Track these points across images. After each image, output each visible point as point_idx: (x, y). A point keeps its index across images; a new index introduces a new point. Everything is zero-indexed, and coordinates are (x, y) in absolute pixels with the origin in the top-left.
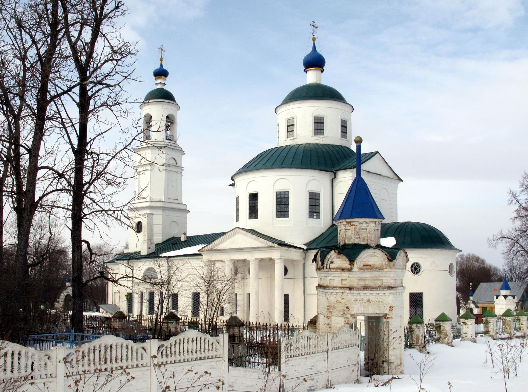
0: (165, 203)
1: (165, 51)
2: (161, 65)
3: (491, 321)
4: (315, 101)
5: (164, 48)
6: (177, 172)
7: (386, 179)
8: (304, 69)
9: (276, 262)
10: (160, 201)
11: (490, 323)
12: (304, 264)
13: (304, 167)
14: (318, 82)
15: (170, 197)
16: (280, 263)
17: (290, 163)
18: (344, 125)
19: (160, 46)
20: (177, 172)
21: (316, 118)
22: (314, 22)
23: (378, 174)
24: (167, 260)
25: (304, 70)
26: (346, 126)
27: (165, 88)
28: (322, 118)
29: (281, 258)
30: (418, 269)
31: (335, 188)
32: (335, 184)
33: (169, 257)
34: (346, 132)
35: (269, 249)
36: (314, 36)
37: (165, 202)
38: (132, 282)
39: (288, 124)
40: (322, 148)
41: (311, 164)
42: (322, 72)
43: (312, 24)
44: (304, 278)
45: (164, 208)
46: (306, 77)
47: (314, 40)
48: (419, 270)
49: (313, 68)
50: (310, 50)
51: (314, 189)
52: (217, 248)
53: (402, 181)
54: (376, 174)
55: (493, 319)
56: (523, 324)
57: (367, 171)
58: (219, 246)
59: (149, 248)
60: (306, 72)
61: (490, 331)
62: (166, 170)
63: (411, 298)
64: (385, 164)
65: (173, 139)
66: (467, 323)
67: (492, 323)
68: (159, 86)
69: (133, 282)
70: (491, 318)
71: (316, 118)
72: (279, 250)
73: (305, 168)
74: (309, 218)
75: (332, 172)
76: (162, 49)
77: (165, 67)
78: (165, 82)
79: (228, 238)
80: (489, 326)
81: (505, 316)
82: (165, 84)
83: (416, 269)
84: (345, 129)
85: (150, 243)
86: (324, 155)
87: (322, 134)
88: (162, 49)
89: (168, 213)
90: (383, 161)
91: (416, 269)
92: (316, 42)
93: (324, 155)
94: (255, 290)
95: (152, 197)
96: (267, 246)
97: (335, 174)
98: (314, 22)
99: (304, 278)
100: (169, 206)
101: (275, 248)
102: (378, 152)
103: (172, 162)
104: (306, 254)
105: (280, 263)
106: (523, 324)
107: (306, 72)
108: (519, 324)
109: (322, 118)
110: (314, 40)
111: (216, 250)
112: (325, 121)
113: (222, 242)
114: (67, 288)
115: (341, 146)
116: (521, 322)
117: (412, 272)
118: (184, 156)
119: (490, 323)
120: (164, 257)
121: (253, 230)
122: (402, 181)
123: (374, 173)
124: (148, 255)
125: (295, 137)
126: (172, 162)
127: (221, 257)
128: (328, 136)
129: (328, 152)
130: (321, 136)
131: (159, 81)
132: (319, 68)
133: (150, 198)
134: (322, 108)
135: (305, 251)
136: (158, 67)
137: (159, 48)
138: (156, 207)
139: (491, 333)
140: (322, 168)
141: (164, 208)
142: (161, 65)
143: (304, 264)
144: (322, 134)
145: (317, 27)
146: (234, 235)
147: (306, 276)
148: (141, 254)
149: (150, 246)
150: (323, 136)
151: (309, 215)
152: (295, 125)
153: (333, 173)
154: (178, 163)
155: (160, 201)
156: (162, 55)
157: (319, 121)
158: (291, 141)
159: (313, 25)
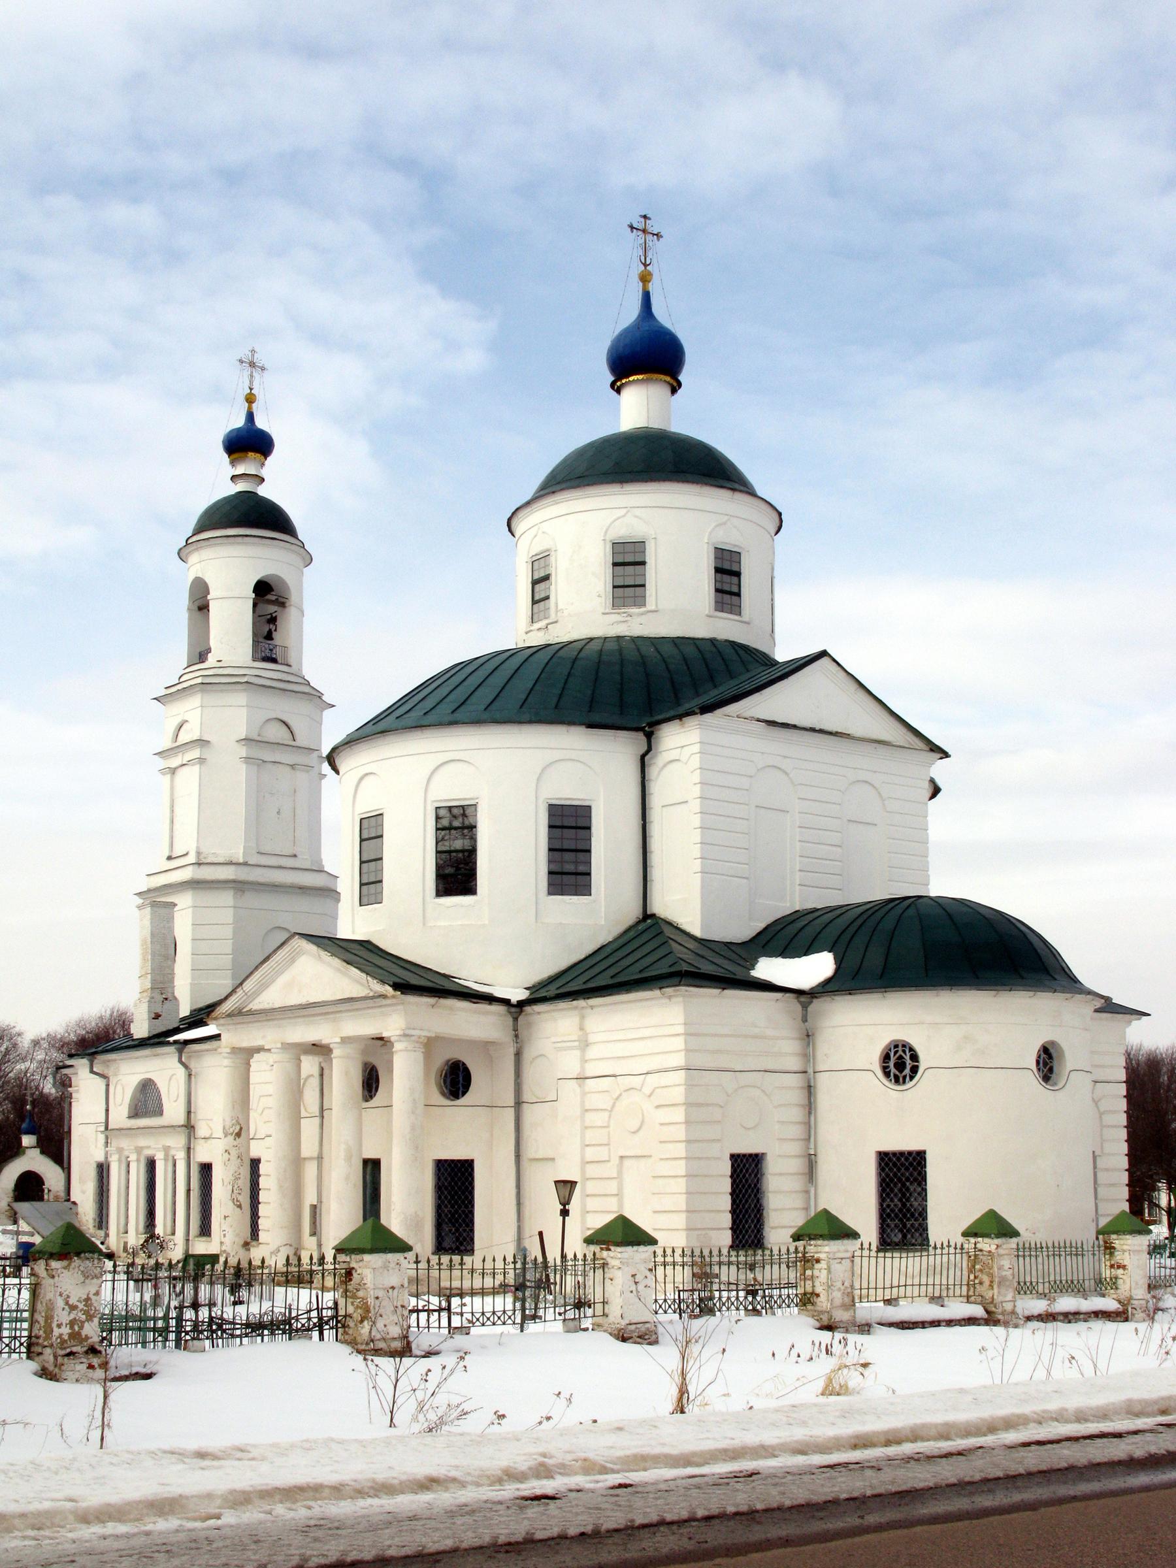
0: (246, 869)
1: (263, 369)
2: (250, 417)
3: (822, 1256)
4: (615, 488)
5: (259, 359)
6: (292, 766)
7: (870, 748)
8: (612, 379)
9: (398, 1046)
10: (231, 863)
11: (818, 1261)
12: (518, 1055)
13: (527, 717)
14: (656, 424)
15: (267, 848)
16: (406, 1050)
17: (483, 707)
18: (727, 566)
19: (244, 353)
20: (292, 766)
21: (618, 546)
22: (645, 217)
23: (830, 733)
24: (180, 1052)
25: (613, 385)
26: (735, 568)
27: (263, 491)
28: (735, 556)
29: (405, 1035)
30: (891, 1064)
31: (655, 789)
32: (653, 772)
33: (187, 1042)
34: (735, 589)
35: (370, 1003)
36: (645, 265)
37: (245, 864)
38: (103, 1129)
39: (536, 577)
40: (644, 650)
41: (556, 707)
42: (674, 391)
43: (638, 223)
44: (518, 1104)
45: (239, 886)
46: (619, 404)
47: (645, 278)
48: (914, 1070)
49: (640, 377)
50: (630, 313)
51: (569, 792)
52: (255, 1005)
53: (945, 755)
54: (821, 731)
55: (827, 1249)
56: (1124, 1267)
57: (771, 723)
58: (257, 1001)
59: (157, 1016)
60: (618, 391)
61: (818, 1295)
62: (248, 759)
63: (920, 1173)
64: (861, 694)
65: (285, 656)
66: (609, 1260)
67: (823, 1265)
68: (241, 487)
69: (107, 1128)
70: (819, 1242)
71: (618, 546)
72: (400, 1007)
73: (530, 722)
74: (551, 893)
75: (637, 729)
76: (252, 364)
77: (261, 423)
78: (264, 473)
79: (280, 973)
80: (816, 1273)
81: (976, 1235)
82: (263, 480)
83: (900, 1065)
84: (735, 579)
85: (160, 998)
86: (622, 674)
87: (640, 601)
88: (252, 364)
89: (252, 900)
90: (853, 686)
91: (900, 1065)
92: (654, 288)
93: (622, 674)
94: (343, 1147)
95: (203, 849)
96: (371, 994)
97: (649, 736)
98: (645, 217)
99: (518, 1104)
100: (261, 880)
101: (388, 1002)
102: (824, 654)
103: (276, 733)
104: (516, 1019)
105: (406, 1050)
106: (1124, 1267)
107: (618, 391)
108: (1112, 1266)
109: (735, 556)
110: (645, 278)
111: (251, 1013)
112: (650, 558)
113: (263, 986)
114: (24, 1153)
115: (713, 641)
116: (1119, 1257)
117: (887, 1074)
118: (327, 713)
119: (818, 1261)
120: (176, 1042)
121: (367, 945)
122: (945, 755)
123: (813, 730)
124: (149, 1038)
125: (553, 618)
126: (276, 733)
127: (264, 1037)
128: (660, 607)
129: (644, 664)
130: (635, 610)
131: (240, 469)
132: (662, 377)
133: (198, 853)
134: (638, 512)
135: (513, 1010)
136: (239, 422)
137: (241, 361)
138: (212, 882)
139: (823, 1302)
140: (596, 718)
141: (239, 886)
142: (250, 417)
143: (518, 1055)
144: (640, 601)
145: (658, 235)
146: (293, 960)
147: (527, 1096)
148: (135, 1038)
149: (158, 1010)
150: (643, 609)
151: (550, 884)
152: (553, 578)
153: (640, 736)
154: (297, 737)
155: (231, 863)
156: (251, 382)
157: (629, 558)
158: (541, 634)
159: (641, 226)
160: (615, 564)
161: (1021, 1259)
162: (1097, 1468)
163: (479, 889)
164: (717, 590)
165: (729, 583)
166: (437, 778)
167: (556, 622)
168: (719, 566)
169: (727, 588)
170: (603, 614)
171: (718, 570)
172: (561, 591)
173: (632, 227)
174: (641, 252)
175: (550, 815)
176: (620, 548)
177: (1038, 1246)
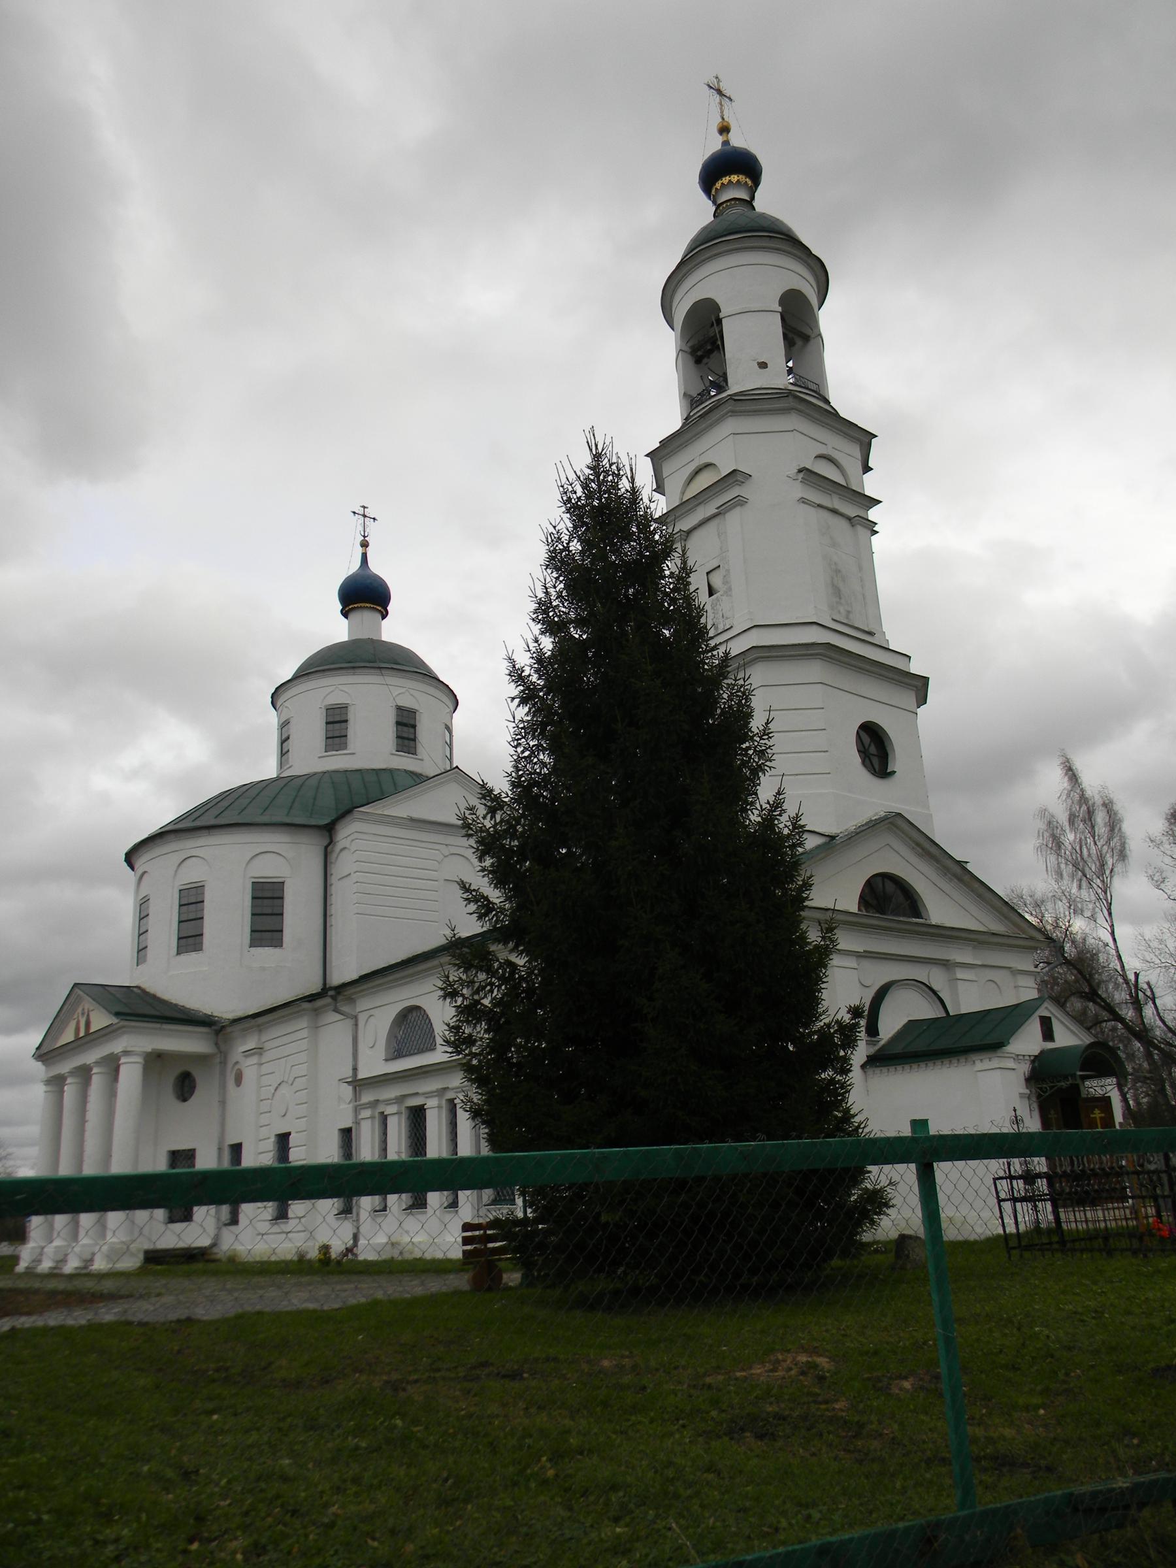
21: (330, 710)
26: (412, 722)
34: (412, 737)
36: (364, 537)
47: (365, 545)
50: (355, 566)
71: (330, 710)
84: (412, 730)
98: (364, 507)
112: (351, 717)
144: (344, 746)
157: (338, 718)
160: (327, 723)
161: (770, 735)
162: (810, 482)
163: (258, 951)
164: (398, 737)
165: (406, 732)
166: (256, 861)
167: (354, 754)
168: (400, 720)
169: (405, 735)
170: (320, 757)
171: (398, 723)
172: (357, 730)
173: (354, 513)
174: (362, 529)
175: (202, 943)
176: (330, 712)
177: (770, 735)
